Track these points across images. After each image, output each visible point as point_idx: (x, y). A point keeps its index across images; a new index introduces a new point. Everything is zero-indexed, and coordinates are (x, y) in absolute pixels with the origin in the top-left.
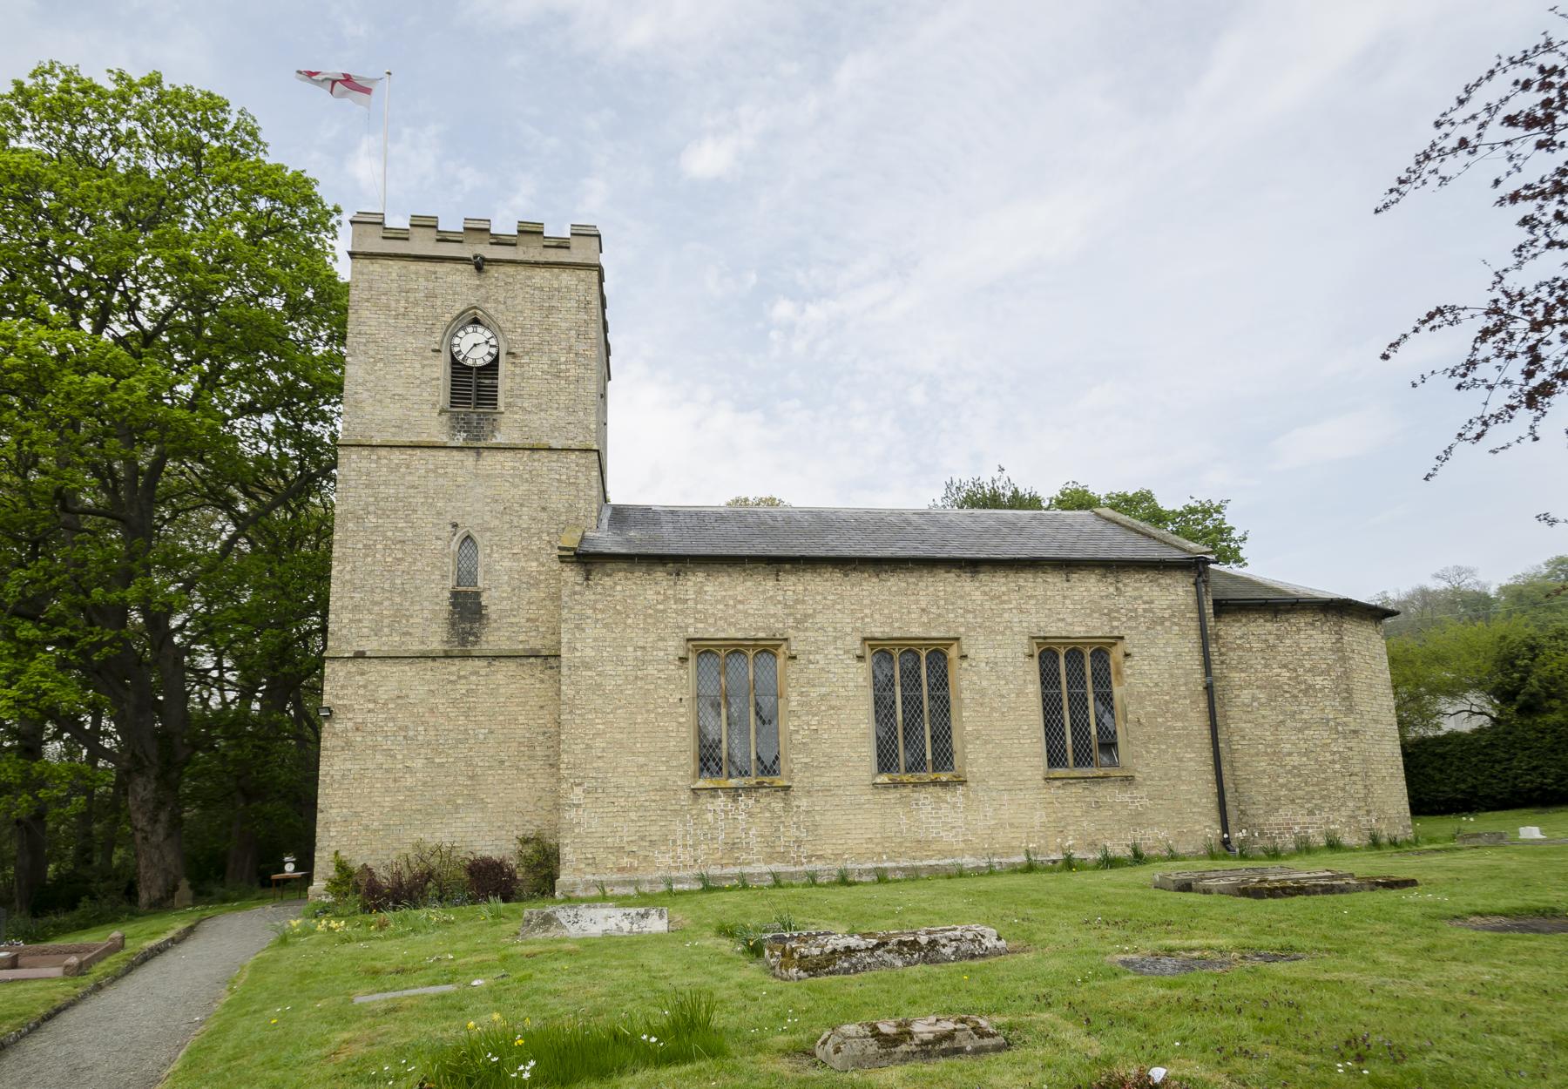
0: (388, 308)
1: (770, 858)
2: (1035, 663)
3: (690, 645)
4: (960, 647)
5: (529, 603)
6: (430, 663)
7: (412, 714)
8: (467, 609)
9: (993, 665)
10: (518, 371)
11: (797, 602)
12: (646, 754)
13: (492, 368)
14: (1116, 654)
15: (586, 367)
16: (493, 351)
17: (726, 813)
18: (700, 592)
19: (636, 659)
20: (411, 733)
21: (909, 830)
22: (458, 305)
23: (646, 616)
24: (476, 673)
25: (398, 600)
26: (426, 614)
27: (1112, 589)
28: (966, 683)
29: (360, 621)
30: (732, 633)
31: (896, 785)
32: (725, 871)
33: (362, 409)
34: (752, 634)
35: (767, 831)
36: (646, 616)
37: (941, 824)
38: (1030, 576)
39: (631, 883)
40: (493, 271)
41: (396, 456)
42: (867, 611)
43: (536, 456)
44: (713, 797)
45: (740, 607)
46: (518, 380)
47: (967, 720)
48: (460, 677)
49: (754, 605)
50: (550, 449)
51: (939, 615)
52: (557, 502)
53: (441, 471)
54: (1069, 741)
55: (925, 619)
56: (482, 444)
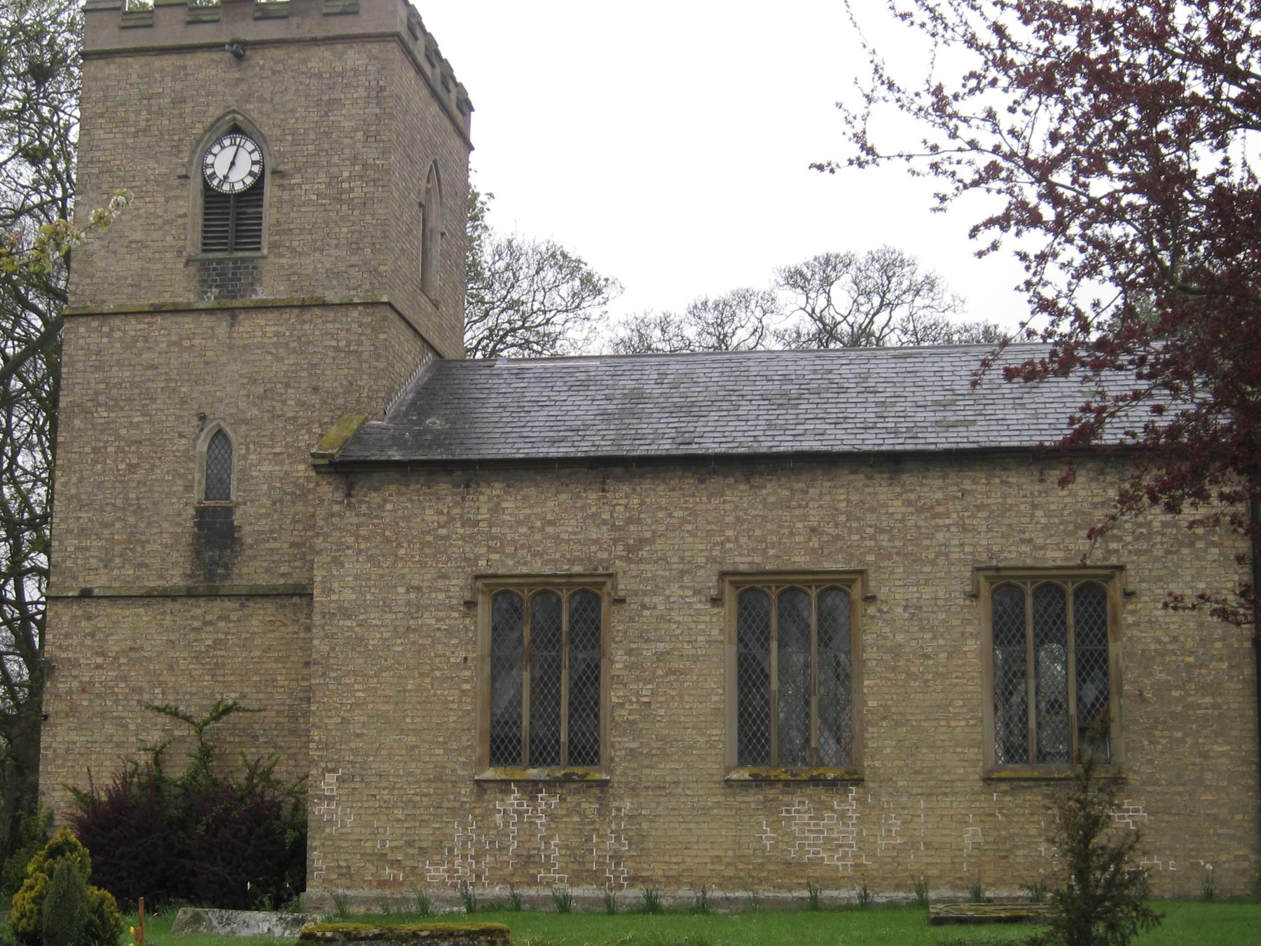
0: (125, 122)
3: (480, 584)
4: (865, 585)
5: (294, 521)
6: (170, 605)
7: (147, 672)
8: (215, 532)
9: (913, 609)
11: (630, 521)
12: (417, 732)
16: (256, 169)
17: (520, 814)
19: (409, 603)
21: (774, 847)
23: (424, 544)
24: (225, 618)
25: (132, 520)
26: (166, 538)
28: (881, 635)
29: (87, 549)
30: (537, 566)
31: (758, 782)
35: (575, 841)
36: (424, 544)
37: (826, 837)
38: (981, 476)
40: (258, 59)
41: (133, 326)
42: (730, 533)
44: (502, 791)
45: (550, 530)
46: (286, 209)
48: (205, 623)
49: (568, 527)
51: (837, 537)
53: (187, 343)
55: (815, 543)
56: (237, 303)
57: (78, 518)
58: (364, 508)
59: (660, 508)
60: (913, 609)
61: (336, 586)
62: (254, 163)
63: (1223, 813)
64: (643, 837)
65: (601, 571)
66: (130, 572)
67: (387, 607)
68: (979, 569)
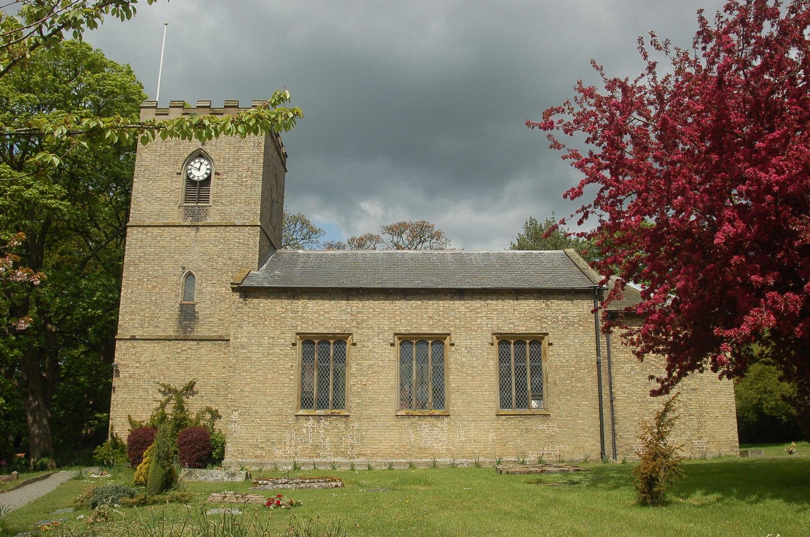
1: (336, 454)
2: (495, 348)
5: (220, 310)
6: (168, 342)
8: (188, 314)
9: (469, 349)
10: (220, 182)
11: (358, 312)
14: (545, 343)
17: (313, 428)
18: (305, 307)
21: (415, 442)
22: (191, 148)
24: (191, 348)
25: (153, 308)
26: (167, 316)
27: (543, 305)
28: (454, 358)
30: (322, 330)
35: (335, 440)
43: (228, 229)
45: (327, 315)
50: (235, 226)
54: (514, 393)
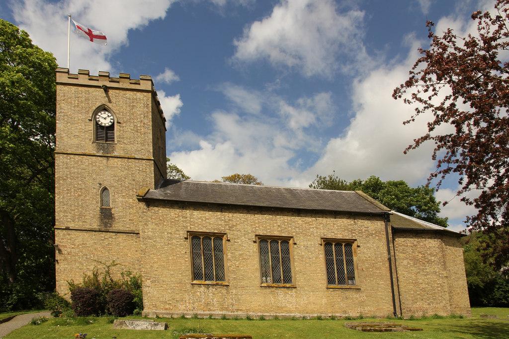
1: (222, 309)
2: (322, 247)
5: (130, 214)
8: (106, 215)
9: (306, 247)
11: (229, 220)
13: (111, 127)
15: (148, 128)
16: (112, 121)
17: (205, 293)
18: (191, 215)
20: (88, 257)
21: (274, 303)
24: (111, 238)
27: (352, 222)
30: (204, 230)
32: (205, 312)
33: (63, 140)
34: (212, 231)
35: (220, 300)
37: (287, 302)
39: (169, 314)
43: (130, 160)
45: (207, 221)
47: (296, 266)
49: (212, 221)
50: (135, 159)
52: (139, 178)
53: (94, 164)
55: (280, 229)
57: (64, 208)
58: (153, 211)
59: (238, 218)
60: (306, 247)
61: (146, 231)
62: (111, 119)
63: (384, 297)
64: (239, 299)
65: (222, 232)
66: (81, 223)
67: (162, 237)
68: (322, 238)
